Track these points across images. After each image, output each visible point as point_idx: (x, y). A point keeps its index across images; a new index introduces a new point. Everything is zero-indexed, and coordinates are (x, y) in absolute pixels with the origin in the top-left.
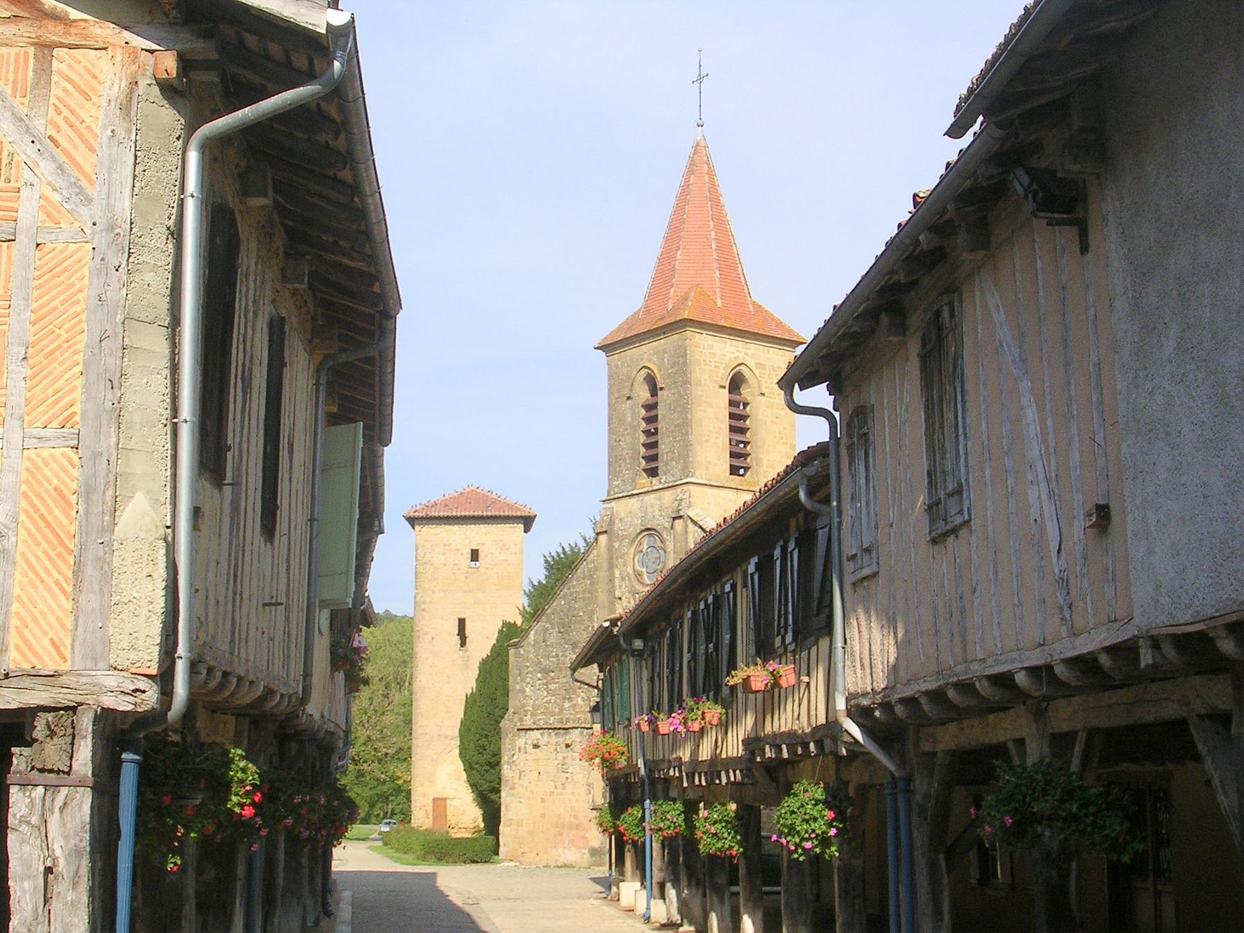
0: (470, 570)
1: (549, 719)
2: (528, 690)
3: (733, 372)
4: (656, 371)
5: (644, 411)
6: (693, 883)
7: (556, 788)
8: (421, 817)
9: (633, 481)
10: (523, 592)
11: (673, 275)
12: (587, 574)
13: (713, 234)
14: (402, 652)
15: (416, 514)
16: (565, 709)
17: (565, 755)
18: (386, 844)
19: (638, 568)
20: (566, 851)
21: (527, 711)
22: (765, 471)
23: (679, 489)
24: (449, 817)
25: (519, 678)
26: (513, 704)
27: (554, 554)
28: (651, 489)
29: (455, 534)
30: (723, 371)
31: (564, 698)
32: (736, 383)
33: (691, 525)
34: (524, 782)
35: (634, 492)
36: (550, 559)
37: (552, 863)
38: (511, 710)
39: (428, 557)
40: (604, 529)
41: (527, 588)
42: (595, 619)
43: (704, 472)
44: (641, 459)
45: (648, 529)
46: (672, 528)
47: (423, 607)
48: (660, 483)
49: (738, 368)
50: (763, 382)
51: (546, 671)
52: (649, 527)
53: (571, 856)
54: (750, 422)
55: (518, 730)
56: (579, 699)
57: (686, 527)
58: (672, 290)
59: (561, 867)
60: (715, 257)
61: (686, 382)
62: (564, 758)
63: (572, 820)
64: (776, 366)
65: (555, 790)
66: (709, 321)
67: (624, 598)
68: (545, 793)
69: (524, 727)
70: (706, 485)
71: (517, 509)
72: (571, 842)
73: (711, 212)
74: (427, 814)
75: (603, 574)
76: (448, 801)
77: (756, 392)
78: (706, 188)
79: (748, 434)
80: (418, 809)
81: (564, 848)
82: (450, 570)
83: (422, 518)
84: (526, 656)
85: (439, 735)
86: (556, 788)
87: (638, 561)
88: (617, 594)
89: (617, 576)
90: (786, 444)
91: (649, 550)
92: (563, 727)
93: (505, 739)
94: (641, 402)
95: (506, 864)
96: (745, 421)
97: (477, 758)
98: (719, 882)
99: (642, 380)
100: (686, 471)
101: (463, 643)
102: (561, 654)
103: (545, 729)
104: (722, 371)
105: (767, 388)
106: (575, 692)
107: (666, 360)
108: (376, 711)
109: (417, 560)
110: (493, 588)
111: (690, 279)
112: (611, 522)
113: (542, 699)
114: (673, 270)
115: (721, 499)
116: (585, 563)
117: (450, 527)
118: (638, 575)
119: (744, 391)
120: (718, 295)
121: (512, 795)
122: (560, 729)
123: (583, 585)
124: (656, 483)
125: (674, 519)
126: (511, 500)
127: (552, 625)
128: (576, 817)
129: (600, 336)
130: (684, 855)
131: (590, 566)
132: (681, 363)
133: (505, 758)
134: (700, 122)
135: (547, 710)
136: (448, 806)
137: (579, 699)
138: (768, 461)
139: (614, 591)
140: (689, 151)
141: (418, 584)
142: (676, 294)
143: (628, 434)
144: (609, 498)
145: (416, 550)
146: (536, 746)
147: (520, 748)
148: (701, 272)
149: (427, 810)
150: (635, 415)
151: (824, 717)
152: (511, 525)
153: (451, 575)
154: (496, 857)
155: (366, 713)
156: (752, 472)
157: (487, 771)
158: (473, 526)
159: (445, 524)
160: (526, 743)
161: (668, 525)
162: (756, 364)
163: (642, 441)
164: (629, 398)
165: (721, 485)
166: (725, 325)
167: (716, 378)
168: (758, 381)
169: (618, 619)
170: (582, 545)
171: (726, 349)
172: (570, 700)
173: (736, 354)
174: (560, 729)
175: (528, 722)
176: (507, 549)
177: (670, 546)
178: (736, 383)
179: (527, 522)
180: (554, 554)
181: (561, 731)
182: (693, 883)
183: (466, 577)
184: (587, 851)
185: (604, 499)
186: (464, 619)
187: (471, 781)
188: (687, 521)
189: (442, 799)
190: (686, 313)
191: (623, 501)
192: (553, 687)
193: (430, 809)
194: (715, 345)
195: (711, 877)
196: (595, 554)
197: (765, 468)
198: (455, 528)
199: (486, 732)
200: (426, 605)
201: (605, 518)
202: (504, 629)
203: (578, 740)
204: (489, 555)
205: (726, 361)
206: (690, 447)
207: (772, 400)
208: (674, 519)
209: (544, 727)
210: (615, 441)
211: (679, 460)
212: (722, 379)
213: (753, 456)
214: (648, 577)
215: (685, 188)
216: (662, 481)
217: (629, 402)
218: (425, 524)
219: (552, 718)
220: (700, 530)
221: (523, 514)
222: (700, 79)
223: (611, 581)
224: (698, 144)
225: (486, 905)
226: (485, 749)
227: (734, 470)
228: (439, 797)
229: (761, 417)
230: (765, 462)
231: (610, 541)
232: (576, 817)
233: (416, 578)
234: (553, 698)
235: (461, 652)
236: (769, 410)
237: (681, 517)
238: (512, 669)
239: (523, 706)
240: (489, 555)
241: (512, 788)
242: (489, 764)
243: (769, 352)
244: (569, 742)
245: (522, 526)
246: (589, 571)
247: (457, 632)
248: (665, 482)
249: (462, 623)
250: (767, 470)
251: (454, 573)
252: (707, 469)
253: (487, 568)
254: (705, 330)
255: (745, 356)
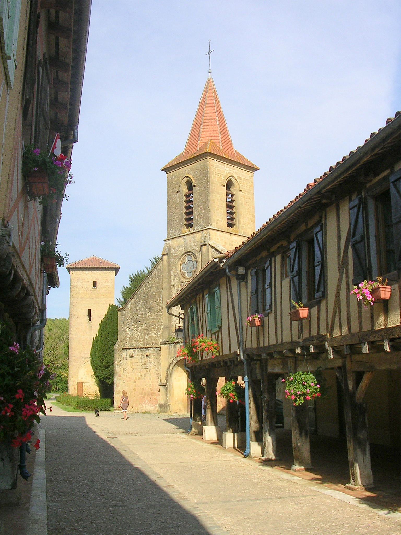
0: (93, 290)
1: (138, 343)
2: (127, 330)
3: (228, 179)
4: (192, 178)
5: (185, 198)
6: (303, 434)
7: (142, 376)
8: (73, 390)
9: (180, 230)
10: (120, 291)
11: (199, 136)
12: (157, 275)
13: (217, 118)
14: (62, 330)
15: (71, 266)
16: (146, 339)
17: (146, 360)
18: (58, 401)
19: (182, 271)
20: (147, 405)
21: (127, 340)
22: (242, 226)
23: (204, 232)
24: (84, 390)
25: (123, 325)
26: (120, 337)
27: (134, 275)
28: (189, 233)
29: (87, 275)
30: (224, 179)
31: (145, 334)
32: (229, 185)
33: (210, 249)
34: (126, 373)
35: (181, 235)
36: (132, 277)
37: (139, 411)
38: (119, 340)
39: (76, 284)
40: (166, 253)
41: (122, 289)
42: (161, 296)
43: (216, 224)
44: (184, 220)
45: (188, 252)
46: (201, 250)
47: (73, 305)
48: (194, 230)
49: (230, 178)
50: (241, 186)
51: (136, 321)
52: (189, 251)
53: (149, 408)
54: (235, 203)
55: (123, 349)
56: (153, 334)
57: (208, 249)
58: (199, 141)
59: (144, 413)
60: (219, 128)
61: (207, 182)
62: (145, 362)
63: (150, 391)
64: (246, 179)
65: (141, 377)
66: (218, 154)
67: (175, 285)
68: (136, 378)
69: (125, 348)
70: (216, 230)
71: (112, 265)
72: (149, 401)
73: (216, 109)
74: (75, 389)
75: (165, 274)
76: (84, 384)
77: (238, 190)
78: (214, 99)
79: (234, 209)
80: (71, 387)
81: (146, 404)
82: (85, 290)
83: (73, 268)
84: (126, 315)
85: (80, 357)
86: (142, 376)
87: (183, 268)
88: (172, 283)
89: (172, 275)
90: (251, 215)
91: (188, 262)
92: (145, 347)
93: (116, 353)
94: (184, 193)
95: (117, 412)
96: (233, 203)
97: (100, 364)
98: (361, 437)
99: (184, 183)
100: (207, 223)
101: (90, 320)
102: (144, 313)
103: (136, 348)
104: (223, 178)
105: (242, 188)
106: (151, 331)
107: (197, 172)
108: (53, 349)
109: (71, 285)
110: (102, 297)
111: (207, 137)
112: (169, 250)
113: (134, 335)
114: (199, 133)
115: (223, 237)
116: (156, 270)
117: (85, 272)
118: (183, 274)
119: (232, 189)
120: (221, 144)
121: (120, 379)
122: (143, 348)
123: (155, 280)
124: (192, 230)
125: (202, 246)
126: (110, 262)
127: (140, 300)
128: (151, 390)
129: (165, 164)
130: (267, 411)
131: (158, 271)
132: (205, 174)
133: (116, 362)
134: (210, 71)
135: (137, 340)
136: (83, 386)
137: (153, 334)
138: (243, 222)
139: (171, 282)
140: (205, 83)
141: (72, 295)
142: (201, 143)
143: (178, 208)
144: (168, 238)
145: (71, 281)
146: (132, 356)
147: (123, 358)
148: (212, 134)
149: (75, 388)
150: (181, 200)
151: (256, 344)
152: (110, 271)
153: (85, 291)
154: (112, 408)
155: (49, 350)
156: (236, 226)
157: (104, 370)
158: (94, 272)
159: (83, 271)
160: (126, 355)
161: (198, 250)
162: (238, 177)
163: (184, 212)
164: (178, 192)
165: (223, 231)
166: (225, 157)
167: (220, 181)
168: (239, 185)
169: (224, 258)
170: (146, 271)
171: (225, 168)
172: (148, 334)
173: (229, 172)
174: (143, 348)
175: (127, 345)
176: (108, 281)
177: (199, 259)
178: (229, 185)
179: (116, 270)
180: (134, 275)
181: (144, 349)
182: (303, 434)
183: (91, 292)
184: (157, 405)
185: (165, 239)
186: (90, 310)
187: (96, 374)
188: (208, 247)
189: (81, 383)
190: (208, 149)
191: (175, 240)
192: (140, 328)
193: (76, 387)
194: (220, 166)
195: (355, 434)
196: (161, 265)
197: (242, 225)
198: (87, 272)
199: (104, 353)
200: (75, 304)
201: (166, 248)
202: (111, 308)
203: (153, 353)
204: (101, 284)
205: (225, 174)
206: (209, 212)
207: (245, 194)
208: (202, 246)
209: (136, 347)
210: (171, 212)
211: (204, 218)
212: (223, 182)
213: (237, 219)
214: (188, 275)
215: (204, 99)
216: (195, 229)
217: (178, 193)
218: (75, 271)
219: (139, 343)
220: (215, 251)
221: (115, 267)
222: (210, 53)
223: (169, 277)
224: (209, 80)
225: (121, 438)
226: (103, 360)
227: (230, 225)
228: (80, 382)
229: (240, 201)
230: (242, 222)
231: (169, 259)
232: (151, 390)
233: (70, 293)
234: (140, 334)
235: (89, 323)
236: (243, 198)
237: (206, 245)
238: (120, 321)
239: (125, 338)
240: (101, 284)
241: (120, 376)
242: (105, 366)
243: (243, 172)
244: (148, 354)
245: (114, 272)
246: (158, 273)
247: (87, 315)
248: (197, 229)
249: (89, 311)
250: (243, 226)
251: (86, 291)
252: (217, 223)
253: (100, 289)
254: (216, 158)
255: (233, 173)
